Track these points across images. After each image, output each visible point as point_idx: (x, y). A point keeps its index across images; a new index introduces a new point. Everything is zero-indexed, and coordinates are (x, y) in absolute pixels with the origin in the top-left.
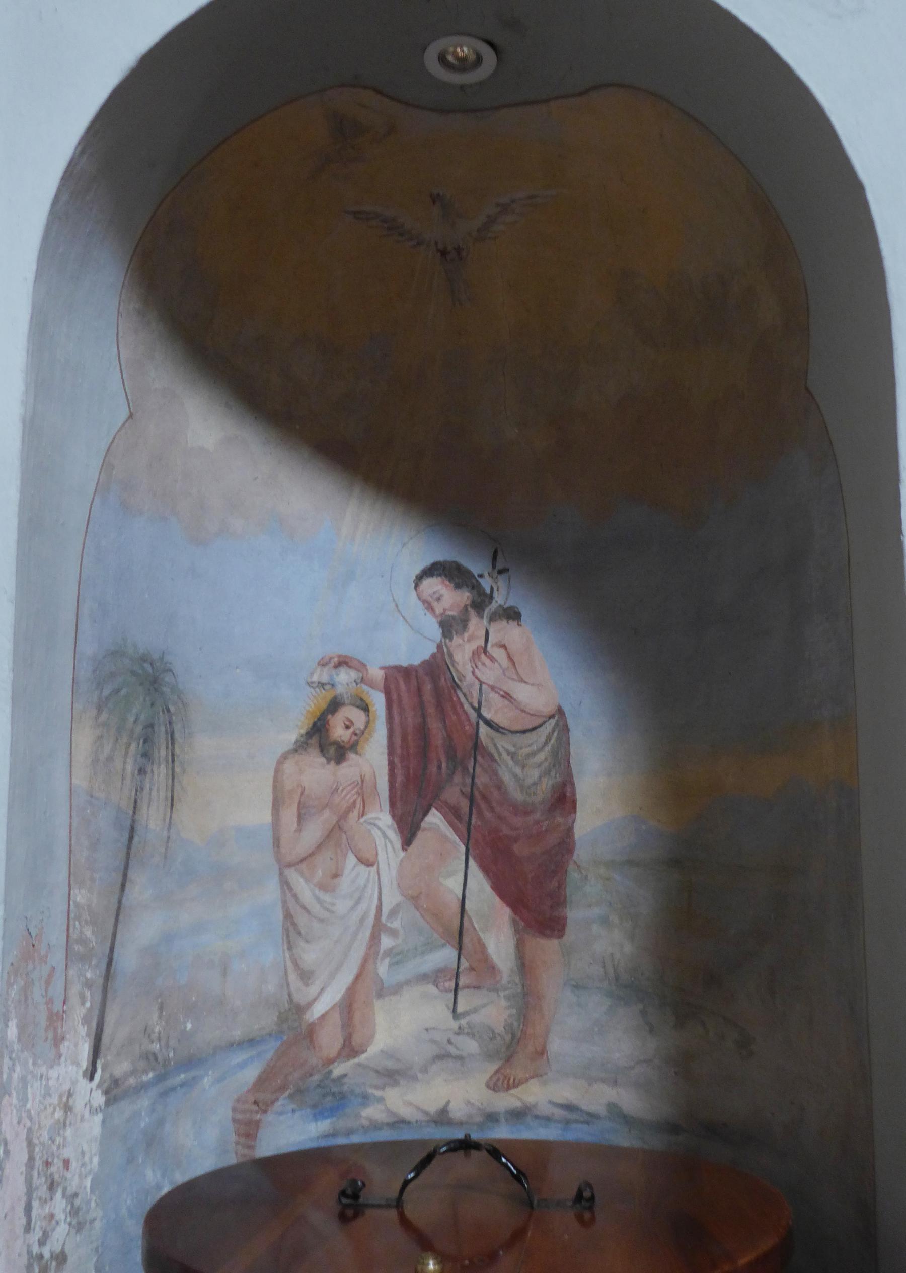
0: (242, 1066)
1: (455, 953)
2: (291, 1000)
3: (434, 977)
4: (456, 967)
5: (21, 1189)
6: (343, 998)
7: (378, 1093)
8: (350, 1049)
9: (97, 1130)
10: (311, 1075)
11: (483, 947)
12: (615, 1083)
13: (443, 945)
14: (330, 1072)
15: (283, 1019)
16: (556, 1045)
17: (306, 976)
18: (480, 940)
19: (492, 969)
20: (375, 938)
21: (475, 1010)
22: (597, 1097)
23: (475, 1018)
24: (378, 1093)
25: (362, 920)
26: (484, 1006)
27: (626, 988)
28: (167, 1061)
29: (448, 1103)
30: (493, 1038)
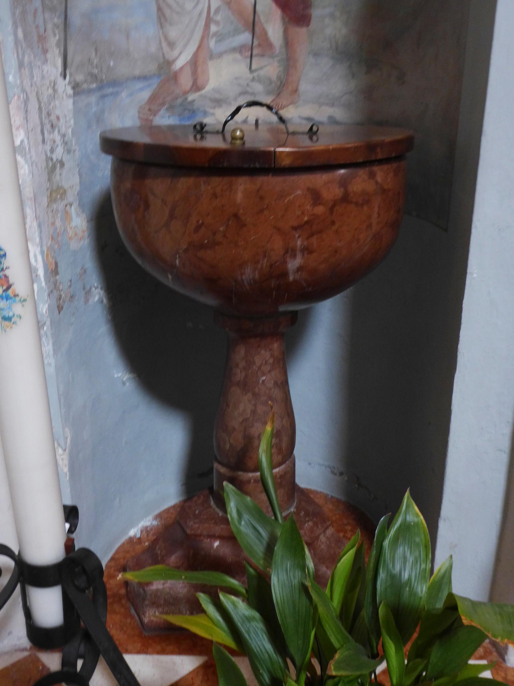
0: (142, 89)
1: (250, 37)
2: (164, 57)
3: (240, 49)
4: (251, 43)
5: (38, 121)
6: (191, 59)
7: (212, 111)
8: (196, 87)
9: (71, 106)
10: (177, 99)
11: (265, 33)
12: (333, 105)
13: (244, 32)
14: (186, 99)
15: (160, 67)
16: (303, 87)
17: (171, 45)
18: (264, 29)
19: (270, 46)
20: (207, 26)
21: (261, 68)
22: (322, 114)
23: (262, 73)
24: (212, 111)
25: (200, 14)
26: (265, 66)
27: (341, 54)
28: (102, 81)
29: (247, 117)
30: (271, 83)
